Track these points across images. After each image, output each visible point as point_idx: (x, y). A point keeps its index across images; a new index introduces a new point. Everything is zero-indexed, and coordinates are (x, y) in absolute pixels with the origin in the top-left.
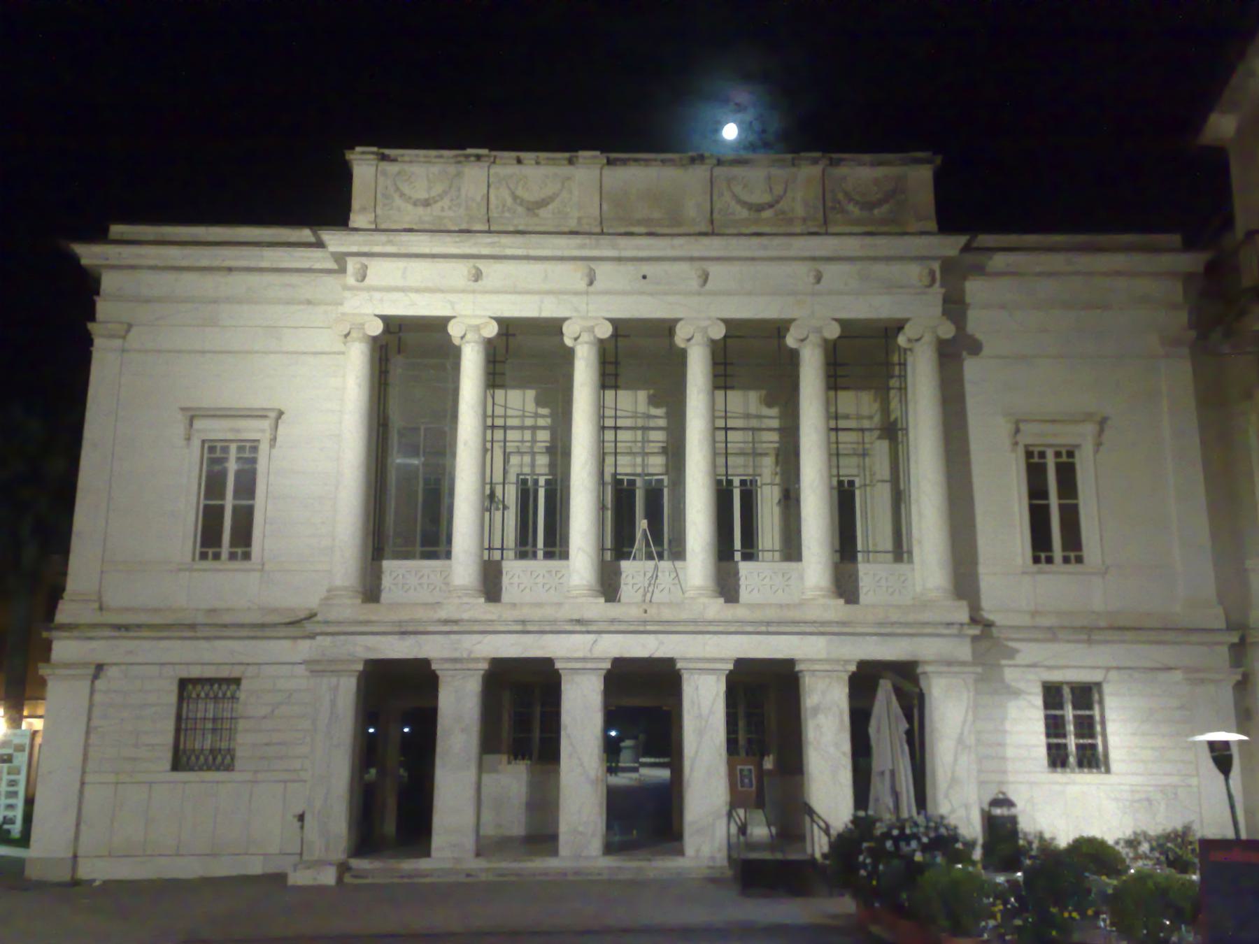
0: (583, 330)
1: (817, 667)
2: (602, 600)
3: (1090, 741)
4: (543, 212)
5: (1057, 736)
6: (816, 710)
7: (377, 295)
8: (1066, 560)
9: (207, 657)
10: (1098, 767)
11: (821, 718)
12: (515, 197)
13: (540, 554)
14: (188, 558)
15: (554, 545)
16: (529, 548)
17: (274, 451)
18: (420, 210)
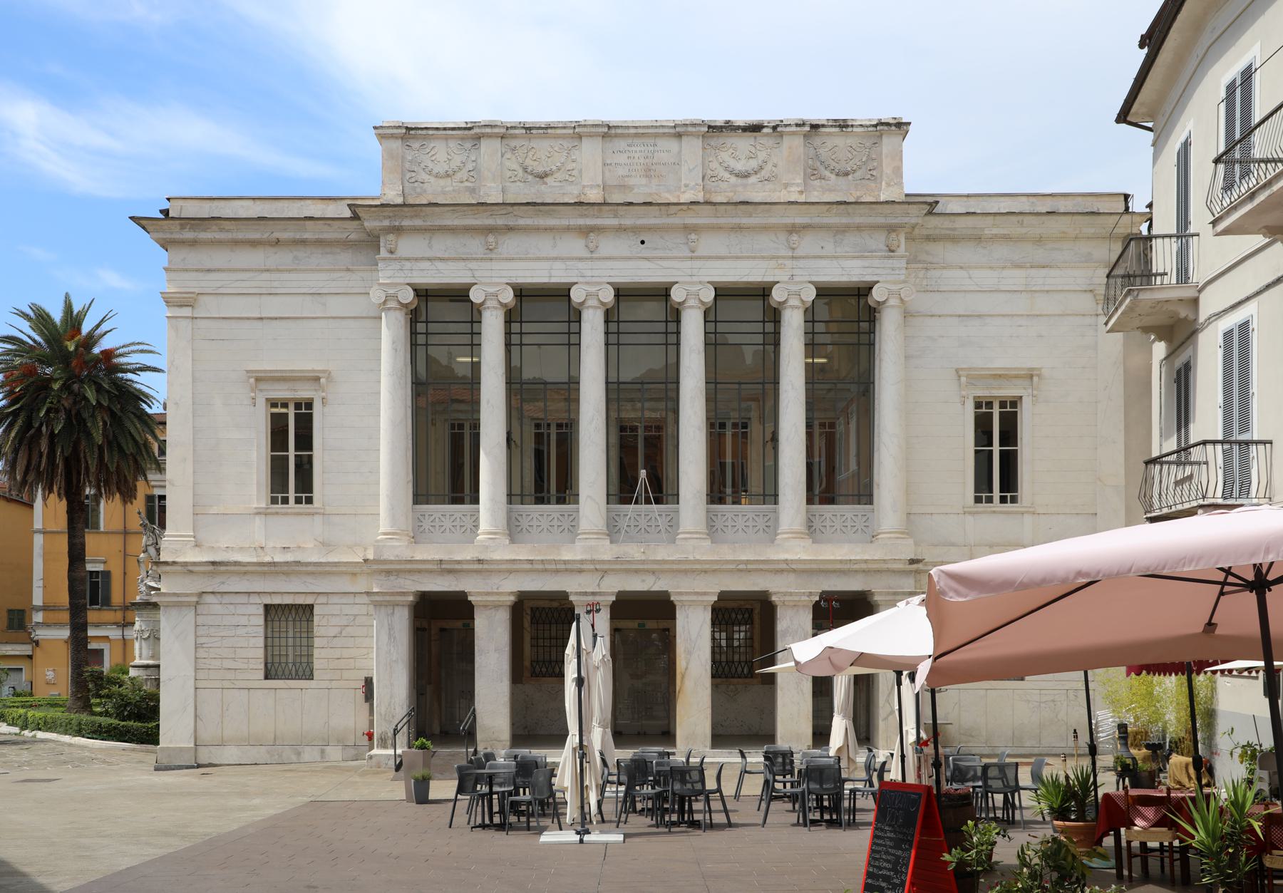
3: (492, 328)
7: (408, 265)
12: (525, 170)
15: (542, 491)
18: (442, 182)
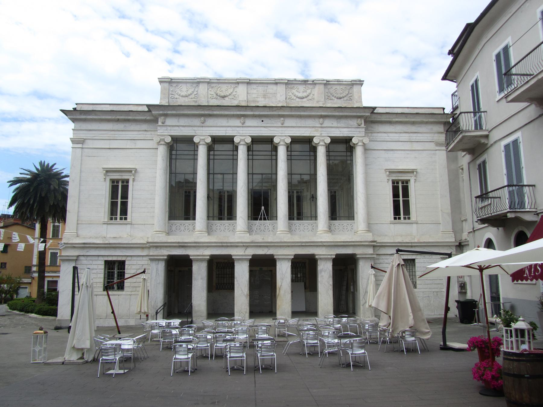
0: (359, 141)
1: (322, 257)
2: (248, 235)
4: (226, 99)
5: (121, 272)
6: (321, 271)
7: (169, 128)
8: (405, 218)
9: (115, 255)
10: (56, 282)
11: (323, 273)
12: (217, 95)
13: (295, 218)
14: (106, 220)
15: (221, 215)
16: (222, 216)
17: (135, 183)
